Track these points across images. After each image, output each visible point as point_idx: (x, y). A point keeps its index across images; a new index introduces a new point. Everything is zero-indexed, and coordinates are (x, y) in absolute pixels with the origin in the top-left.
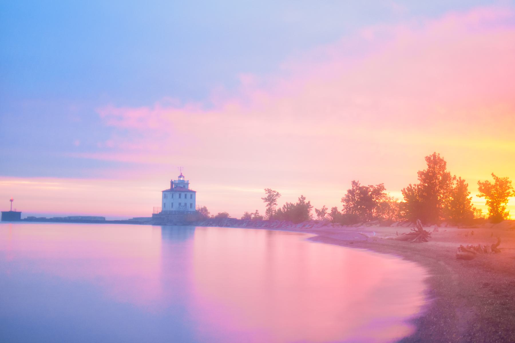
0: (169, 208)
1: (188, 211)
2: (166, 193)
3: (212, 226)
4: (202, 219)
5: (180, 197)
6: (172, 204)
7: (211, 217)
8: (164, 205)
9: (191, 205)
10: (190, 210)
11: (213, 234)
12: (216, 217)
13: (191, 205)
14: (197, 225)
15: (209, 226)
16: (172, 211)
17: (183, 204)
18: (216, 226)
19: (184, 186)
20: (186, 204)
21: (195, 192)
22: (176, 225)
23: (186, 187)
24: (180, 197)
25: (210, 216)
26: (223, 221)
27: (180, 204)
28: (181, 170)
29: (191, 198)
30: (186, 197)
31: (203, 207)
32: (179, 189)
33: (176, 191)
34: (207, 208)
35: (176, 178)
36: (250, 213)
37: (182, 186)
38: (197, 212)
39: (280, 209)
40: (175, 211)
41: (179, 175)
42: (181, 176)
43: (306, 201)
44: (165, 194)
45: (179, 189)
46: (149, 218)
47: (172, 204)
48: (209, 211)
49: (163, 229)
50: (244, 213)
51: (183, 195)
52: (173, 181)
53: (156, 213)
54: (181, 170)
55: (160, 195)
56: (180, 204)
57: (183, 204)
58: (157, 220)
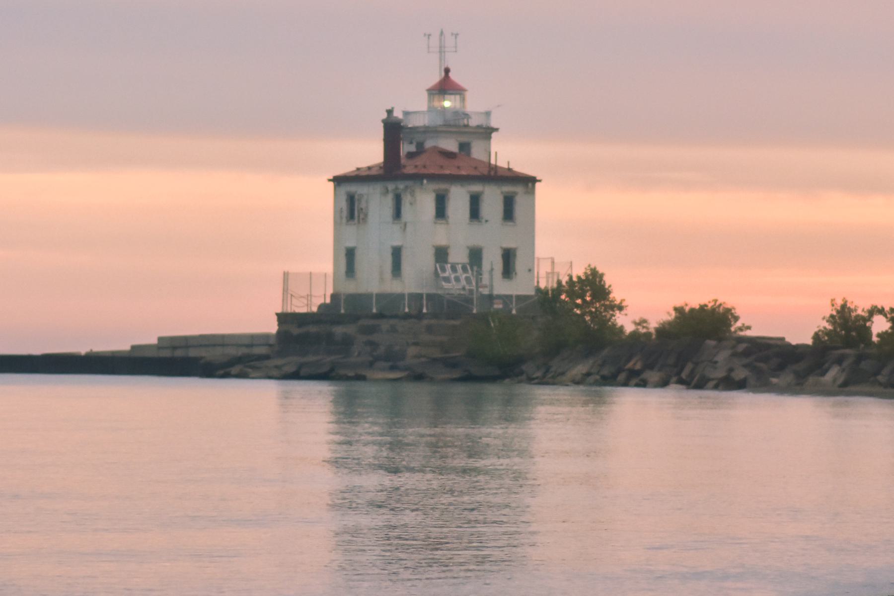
0: (373, 280)
1: (491, 298)
2: (353, 188)
3: (643, 384)
4: (575, 342)
5: (441, 212)
6: (397, 253)
7: (629, 328)
8: (349, 259)
9: (508, 257)
10: (502, 288)
11: (646, 426)
12: (664, 332)
13: (508, 257)
14: (548, 379)
15: (626, 384)
16: (401, 296)
17: (458, 256)
18: (664, 384)
19: (465, 147)
20: (476, 255)
21: (529, 182)
22: (419, 377)
23: (477, 152)
24: (441, 212)
25: (625, 322)
26: (700, 352)
27: (441, 254)
28: (442, 51)
29: (509, 214)
30: (475, 214)
31: (579, 271)
32: (427, 161)
33: (417, 178)
34: (608, 281)
35: (414, 103)
36: (860, 305)
37: (451, 145)
38: (548, 301)
39: (736, 319)
40: (416, 298)
41: (435, 78)
42: (445, 86)
43: (839, 302)
44: (351, 199)
45: (427, 161)
46: (253, 340)
47: (397, 253)
48: (616, 295)
49: (348, 410)
50: (829, 311)
51: (459, 199)
52: (398, 114)
53: (300, 307)
54: (442, 51)
55: (323, 199)
56: (441, 254)
57: (458, 256)
58: (307, 347)
